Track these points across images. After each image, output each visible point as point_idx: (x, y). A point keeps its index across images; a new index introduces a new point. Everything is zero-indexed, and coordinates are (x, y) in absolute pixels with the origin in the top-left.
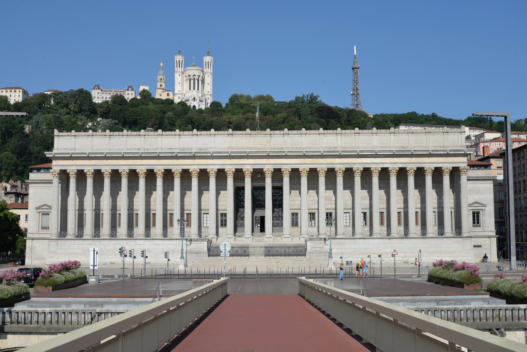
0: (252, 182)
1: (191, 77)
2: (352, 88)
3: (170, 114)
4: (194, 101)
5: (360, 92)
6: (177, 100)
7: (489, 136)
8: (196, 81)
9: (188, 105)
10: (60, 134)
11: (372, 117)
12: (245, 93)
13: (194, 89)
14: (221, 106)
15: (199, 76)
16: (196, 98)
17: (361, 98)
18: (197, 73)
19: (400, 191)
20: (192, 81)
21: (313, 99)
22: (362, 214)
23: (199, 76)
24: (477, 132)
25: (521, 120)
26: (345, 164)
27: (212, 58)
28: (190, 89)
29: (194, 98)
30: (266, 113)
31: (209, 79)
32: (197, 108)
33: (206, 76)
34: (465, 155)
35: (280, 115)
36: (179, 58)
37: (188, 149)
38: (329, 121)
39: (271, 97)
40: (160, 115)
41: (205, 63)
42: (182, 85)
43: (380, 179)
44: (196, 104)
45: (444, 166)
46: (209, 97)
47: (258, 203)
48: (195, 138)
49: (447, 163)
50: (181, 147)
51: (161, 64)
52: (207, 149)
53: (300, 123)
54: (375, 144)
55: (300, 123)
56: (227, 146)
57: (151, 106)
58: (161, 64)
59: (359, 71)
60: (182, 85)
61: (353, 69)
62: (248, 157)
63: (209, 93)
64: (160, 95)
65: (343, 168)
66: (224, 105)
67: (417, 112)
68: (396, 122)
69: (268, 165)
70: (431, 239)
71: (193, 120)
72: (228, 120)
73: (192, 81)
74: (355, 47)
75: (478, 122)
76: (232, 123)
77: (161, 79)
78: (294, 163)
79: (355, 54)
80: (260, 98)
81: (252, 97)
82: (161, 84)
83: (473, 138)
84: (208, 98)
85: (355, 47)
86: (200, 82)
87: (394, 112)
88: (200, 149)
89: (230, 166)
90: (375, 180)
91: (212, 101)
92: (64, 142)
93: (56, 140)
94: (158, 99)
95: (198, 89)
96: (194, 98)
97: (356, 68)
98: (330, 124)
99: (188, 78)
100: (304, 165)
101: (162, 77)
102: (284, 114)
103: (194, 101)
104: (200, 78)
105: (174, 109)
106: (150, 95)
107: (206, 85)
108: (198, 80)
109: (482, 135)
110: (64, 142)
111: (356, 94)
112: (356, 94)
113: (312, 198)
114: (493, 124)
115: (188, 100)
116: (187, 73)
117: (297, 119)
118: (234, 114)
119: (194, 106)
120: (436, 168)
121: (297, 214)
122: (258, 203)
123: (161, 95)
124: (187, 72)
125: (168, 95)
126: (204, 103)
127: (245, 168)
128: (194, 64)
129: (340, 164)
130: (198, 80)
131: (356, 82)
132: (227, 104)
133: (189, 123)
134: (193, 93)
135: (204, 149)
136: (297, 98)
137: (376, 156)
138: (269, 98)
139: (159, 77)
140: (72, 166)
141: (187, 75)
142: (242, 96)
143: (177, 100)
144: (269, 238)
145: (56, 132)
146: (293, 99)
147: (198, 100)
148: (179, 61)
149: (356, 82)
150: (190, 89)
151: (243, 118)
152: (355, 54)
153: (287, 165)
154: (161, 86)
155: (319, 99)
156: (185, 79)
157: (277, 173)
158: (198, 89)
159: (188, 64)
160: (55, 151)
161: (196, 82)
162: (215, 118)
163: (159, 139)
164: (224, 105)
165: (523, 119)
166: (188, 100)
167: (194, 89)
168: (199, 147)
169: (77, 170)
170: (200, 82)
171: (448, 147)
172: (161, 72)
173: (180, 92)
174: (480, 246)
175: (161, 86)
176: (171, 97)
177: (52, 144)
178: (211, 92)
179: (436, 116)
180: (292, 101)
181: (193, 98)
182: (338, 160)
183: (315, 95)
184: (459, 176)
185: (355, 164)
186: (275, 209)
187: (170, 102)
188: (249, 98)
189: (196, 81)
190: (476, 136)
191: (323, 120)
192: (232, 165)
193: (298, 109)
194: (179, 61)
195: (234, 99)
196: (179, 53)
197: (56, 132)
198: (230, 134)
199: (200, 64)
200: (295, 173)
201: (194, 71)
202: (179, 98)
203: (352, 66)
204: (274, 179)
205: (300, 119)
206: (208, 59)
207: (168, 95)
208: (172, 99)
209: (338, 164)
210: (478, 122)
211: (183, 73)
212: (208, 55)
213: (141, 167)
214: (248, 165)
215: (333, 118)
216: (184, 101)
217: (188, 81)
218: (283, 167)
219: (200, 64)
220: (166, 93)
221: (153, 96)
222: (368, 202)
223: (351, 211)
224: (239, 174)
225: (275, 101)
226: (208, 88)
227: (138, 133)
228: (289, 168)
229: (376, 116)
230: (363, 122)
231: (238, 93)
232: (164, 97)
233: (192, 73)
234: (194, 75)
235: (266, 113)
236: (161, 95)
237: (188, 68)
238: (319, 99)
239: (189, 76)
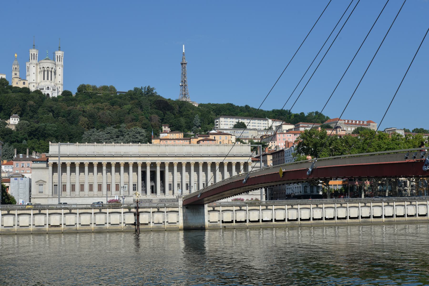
0: (160, 168)
1: (46, 69)
2: (180, 80)
3: (31, 102)
4: (48, 89)
5: (187, 83)
6: (32, 89)
7: (286, 127)
8: (50, 73)
9: (43, 93)
10: (52, 144)
11: (196, 105)
12: (92, 84)
13: (48, 79)
14: (72, 95)
15: (52, 68)
16: (50, 87)
17: (189, 88)
18: (51, 66)
19: (220, 173)
20: (46, 73)
21: (149, 91)
23: (52, 68)
24: (278, 123)
25: (313, 112)
27: (63, 53)
28: (44, 79)
29: (48, 88)
30: (113, 104)
31: (60, 71)
32: (51, 96)
33: (58, 68)
34: (251, 156)
35: (126, 107)
36: (33, 52)
37: (119, 152)
38: (165, 112)
39: (114, 88)
40: (22, 102)
41: (56, 57)
42: (37, 76)
43: (211, 167)
44: (49, 92)
45: (241, 161)
46: (60, 86)
47: (153, 178)
48: (122, 147)
49: (242, 160)
50: (115, 151)
51: (16, 55)
52: (128, 152)
53: (143, 114)
54: (209, 151)
55: (143, 114)
56: (138, 151)
57: (13, 95)
58: (16, 55)
59: (186, 66)
60: (37, 76)
61: (182, 64)
62: (148, 157)
63: (60, 83)
64: (16, 83)
65: (194, 162)
66: (74, 94)
67: (234, 104)
68: (217, 112)
69: (158, 161)
71: (53, 109)
72: (82, 109)
73: (46, 73)
74: (184, 46)
75: (281, 115)
76: (86, 112)
77: (16, 68)
79: (184, 51)
80: (105, 88)
81: (98, 87)
82: (16, 72)
83: (274, 128)
84: (60, 87)
85: (184, 46)
86: (53, 73)
87: (215, 102)
88: (125, 153)
89: (140, 161)
90: (209, 168)
91: (62, 91)
92: (54, 148)
93: (50, 147)
94: (16, 87)
95: (51, 80)
96: (48, 88)
97: (184, 64)
98: (166, 115)
99: (42, 69)
100: (176, 161)
101: (16, 67)
102: (129, 106)
103: (48, 89)
104: (53, 70)
105: (33, 97)
106: (7, 83)
107: (57, 75)
108: (51, 72)
109: (280, 127)
110: (54, 148)
111: (184, 86)
112: (184, 86)
113: (178, 176)
114: (291, 115)
115: (43, 89)
116: (42, 65)
117: (139, 111)
118: (86, 104)
119: (48, 94)
120: (237, 162)
121: (90, 190)
122: (153, 178)
123: (17, 84)
124: (41, 64)
125: (24, 83)
126: (56, 91)
127: (147, 162)
128: (47, 57)
130: (51, 72)
131: (184, 75)
132: (76, 94)
133: (49, 111)
134: (47, 83)
135: (127, 152)
136: (136, 89)
137: (209, 157)
138: (112, 89)
139: (14, 67)
140: (59, 161)
141: (42, 67)
142: (89, 86)
143: (32, 89)
144: (159, 195)
145: (50, 143)
146: (133, 89)
147: (51, 89)
149: (184, 75)
150: (44, 79)
151: (94, 108)
152: (184, 51)
153: (167, 160)
154: (16, 74)
155: (154, 91)
156: (39, 70)
157: (163, 165)
158: (51, 80)
159: (41, 57)
160: (50, 153)
161: (48, 73)
162: (71, 107)
163: (104, 147)
164: (74, 94)
165: (315, 111)
166: (43, 89)
167: (48, 79)
168: (124, 151)
170: (53, 73)
171: (242, 152)
172: (16, 62)
173: (35, 81)
175: (16, 74)
176: (26, 86)
177: (48, 150)
178: (62, 82)
179: (249, 107)
180: (131, 91)
182: (191, 158)
183: (151, 87)
184: (248, 166)
187: (26, 90)
188: (94, 88)
189: (50, 73)
190: (276, 127)
191: (161, 112)
193: (139, 102)
194: (34, 54)
195: (82, 89)
196: (34, 47)
197: (50, 143)
199: (53, 58)
200: (171, 165)
201: (47, 64)
202: (34, 86)
203: (180, 61)
204: (161, 167)
205: (142, 111)
206: (59, 53)
207: (24, 83)
208: (28, 87)
210: (281, 115)
211: (37, 65)
212: (59, 50)
214: (149, 161)
215: (168, 110)
217: (42, 73)
218: (165, 162)
219: (53, 58)
220: (22, 82)
221: (10, 84)
222: (205, 178)
223: (197, 183)
224: (144, 165)
225: (117, 91)
226: (59, 78)
227: (93, 144)
228: (168, 162)
229: (201, 105)
230: (192, 114)
231: (86, 84)
232: (21, 85)
233: (46, 65)
234: (48, 67)
235: (113, 104)
236: (17, 84)
237: (43, 61)
238: (154, 91)
239: (43, 67)
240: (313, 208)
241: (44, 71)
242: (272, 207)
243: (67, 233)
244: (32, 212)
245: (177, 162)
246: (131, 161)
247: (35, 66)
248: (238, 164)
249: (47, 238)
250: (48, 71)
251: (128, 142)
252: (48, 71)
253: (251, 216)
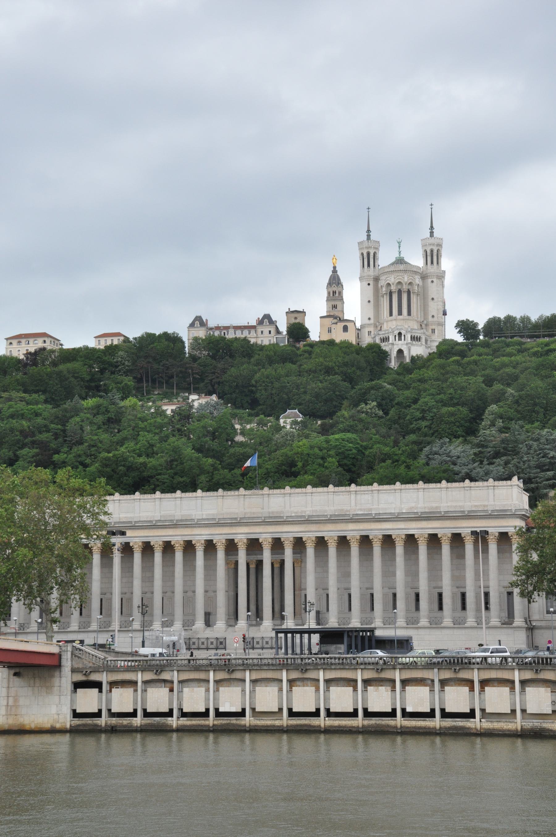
1: (393, 288)
4: (400, 339)
13: (400, 313)
16: (403, 332)
22: (529, 690)
23: (410, 284)
26: (381, 530)
28: (391, 314)
29: (400, 334)
69: (266, 535)
70: (470, 630)
78: (296, 530)
89: (219, 536)
95: (409, 313)
96: (400, 334)
100: (309, 533)
103: (400, 339)
129: (353, 530)
134: (391, 325)
148: (432, 251)
150: (391, 314)
158: (409, 313)
167: (400, 313)
169: (338, 536)
173: (430, 319)
174: (500, 641)
181: (396, 332)
182: (351, 526)
185: (372, 530)
186: (482, 720)
192: (221, 534)
194: (432, 251)
198: (220, 496)
202: (369, 333)
209: (217, 534)
213: (264, 536)
214: (241, 535)
216: (378, 341)
234: (399, 283)
239: (389, 284)
240: (180, 682)
241: (391, 294)
242: (510, 672)
243: (452, 735)
244: (140, 677)
245: (336, 534)
246: (199, 536)
247: (371, 283)
248: (210, 546)
249: (285, 748)
250: (400, 292)
251: (391, 482)
252: (400, 292)
253: (257, 701)
